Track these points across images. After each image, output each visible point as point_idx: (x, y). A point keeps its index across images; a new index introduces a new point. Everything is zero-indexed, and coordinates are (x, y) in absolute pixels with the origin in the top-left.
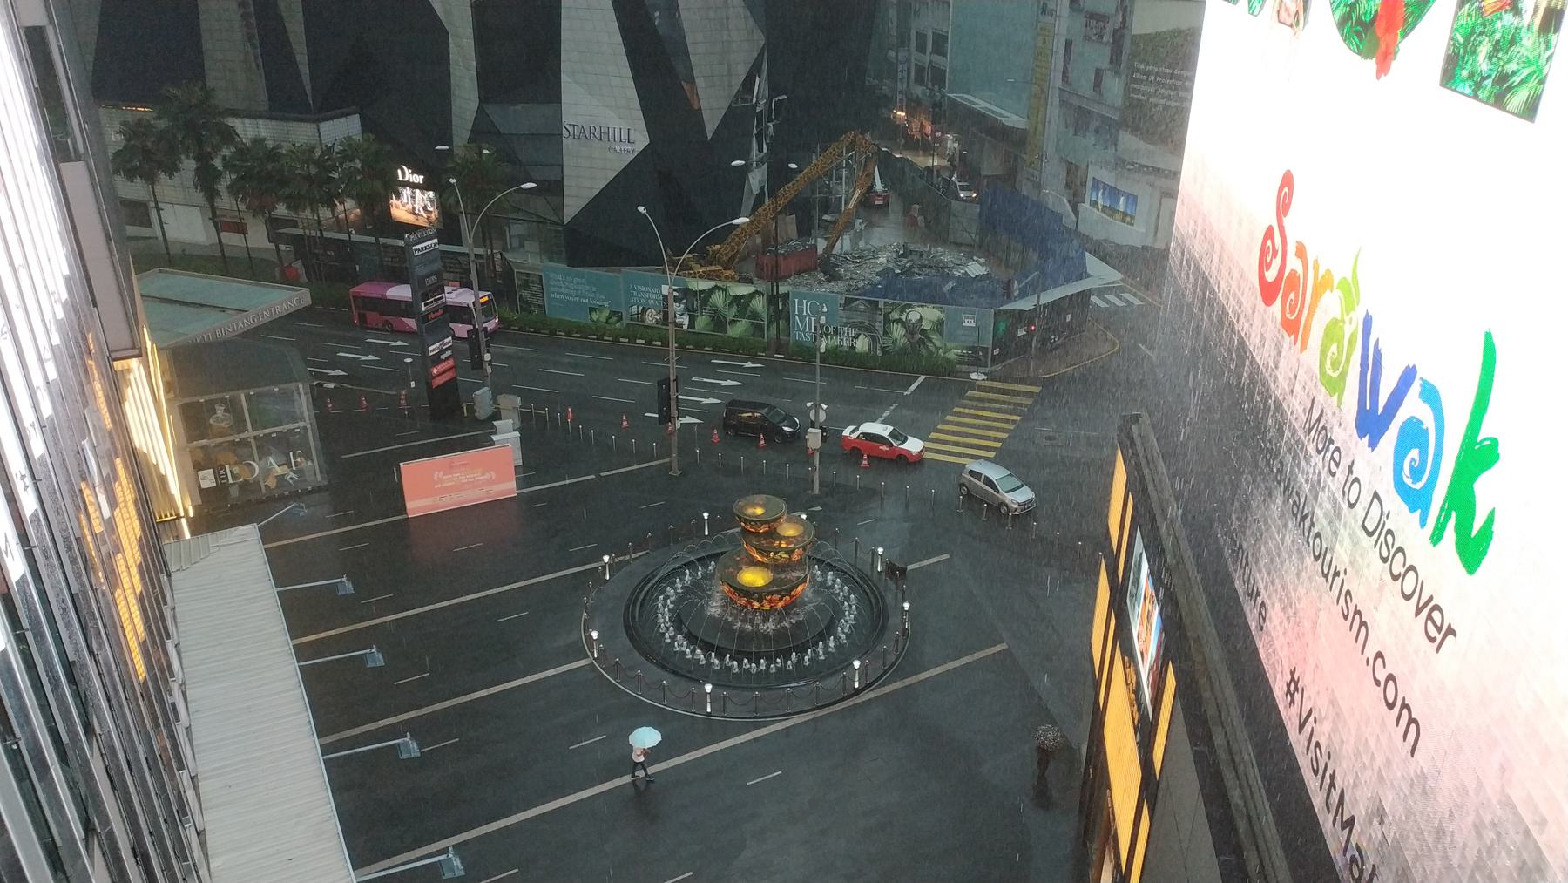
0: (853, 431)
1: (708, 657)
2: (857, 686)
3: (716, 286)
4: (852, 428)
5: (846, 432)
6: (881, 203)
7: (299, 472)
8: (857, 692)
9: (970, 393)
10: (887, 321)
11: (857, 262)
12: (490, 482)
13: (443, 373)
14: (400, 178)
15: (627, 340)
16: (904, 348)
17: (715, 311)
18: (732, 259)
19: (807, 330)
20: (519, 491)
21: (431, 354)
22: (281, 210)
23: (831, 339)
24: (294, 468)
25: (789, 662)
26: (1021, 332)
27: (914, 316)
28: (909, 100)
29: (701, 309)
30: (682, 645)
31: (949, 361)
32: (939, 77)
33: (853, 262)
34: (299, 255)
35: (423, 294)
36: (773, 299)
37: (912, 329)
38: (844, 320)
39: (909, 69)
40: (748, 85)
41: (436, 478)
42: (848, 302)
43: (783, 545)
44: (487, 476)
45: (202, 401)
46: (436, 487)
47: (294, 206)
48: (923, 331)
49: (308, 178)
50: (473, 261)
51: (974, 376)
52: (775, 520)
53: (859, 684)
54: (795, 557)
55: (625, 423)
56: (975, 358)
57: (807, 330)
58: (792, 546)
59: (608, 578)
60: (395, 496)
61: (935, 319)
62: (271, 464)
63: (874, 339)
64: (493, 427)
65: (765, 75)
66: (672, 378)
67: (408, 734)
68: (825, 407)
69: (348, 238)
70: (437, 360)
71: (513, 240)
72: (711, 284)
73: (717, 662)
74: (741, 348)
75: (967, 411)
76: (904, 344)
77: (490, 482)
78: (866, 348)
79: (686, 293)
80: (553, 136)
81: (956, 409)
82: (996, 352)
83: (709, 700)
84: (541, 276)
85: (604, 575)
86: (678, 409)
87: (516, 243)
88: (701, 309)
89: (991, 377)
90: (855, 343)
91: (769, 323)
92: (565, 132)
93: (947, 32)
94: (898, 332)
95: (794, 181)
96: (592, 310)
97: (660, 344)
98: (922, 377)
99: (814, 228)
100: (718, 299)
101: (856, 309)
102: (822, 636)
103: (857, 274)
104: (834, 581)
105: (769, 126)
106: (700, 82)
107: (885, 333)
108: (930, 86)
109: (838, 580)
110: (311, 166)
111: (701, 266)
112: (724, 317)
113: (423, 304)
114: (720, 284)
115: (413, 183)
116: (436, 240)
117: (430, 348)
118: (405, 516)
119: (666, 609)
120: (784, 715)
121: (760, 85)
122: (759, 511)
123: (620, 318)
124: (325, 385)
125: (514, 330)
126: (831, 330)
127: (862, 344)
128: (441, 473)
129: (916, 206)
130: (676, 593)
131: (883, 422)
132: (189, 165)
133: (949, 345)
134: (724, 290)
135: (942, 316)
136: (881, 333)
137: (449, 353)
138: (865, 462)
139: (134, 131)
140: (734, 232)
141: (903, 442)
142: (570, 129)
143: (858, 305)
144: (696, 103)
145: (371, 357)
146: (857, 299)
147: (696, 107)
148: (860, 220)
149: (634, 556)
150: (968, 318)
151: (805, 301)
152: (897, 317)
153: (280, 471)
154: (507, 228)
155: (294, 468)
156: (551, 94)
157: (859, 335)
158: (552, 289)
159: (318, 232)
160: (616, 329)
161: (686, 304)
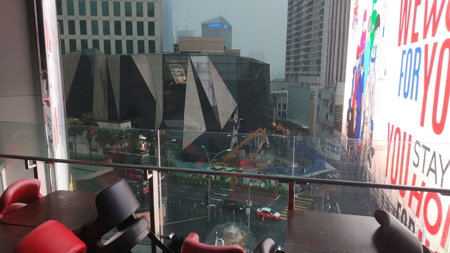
0: (260, 210)
5: (258, 210)
18: (227, 161)
21: (144, 185)
23: (254, 183)
32: (284, 114)
40: (233, 116)
55: (195, 206)
63: (266, 184)
65: (237, 114)
68: (251, 202)
78: (264, 186)
82: (301, 189)
84: (175, 164)
89: (300, 196)
90: (261, 185)
92: (184, 127)
98: (280, 195)
107: (269, 182)
108: (282, 117)
114: (223, 167)
117: (144, 183)
121: (236, 116)
131: (268, 208)
136: (268, 182)
138: (263, 219)
141: (274, 214)
146: (261, 173)
148: (263, 151)
156: (182, 118)
157: (262, 182)
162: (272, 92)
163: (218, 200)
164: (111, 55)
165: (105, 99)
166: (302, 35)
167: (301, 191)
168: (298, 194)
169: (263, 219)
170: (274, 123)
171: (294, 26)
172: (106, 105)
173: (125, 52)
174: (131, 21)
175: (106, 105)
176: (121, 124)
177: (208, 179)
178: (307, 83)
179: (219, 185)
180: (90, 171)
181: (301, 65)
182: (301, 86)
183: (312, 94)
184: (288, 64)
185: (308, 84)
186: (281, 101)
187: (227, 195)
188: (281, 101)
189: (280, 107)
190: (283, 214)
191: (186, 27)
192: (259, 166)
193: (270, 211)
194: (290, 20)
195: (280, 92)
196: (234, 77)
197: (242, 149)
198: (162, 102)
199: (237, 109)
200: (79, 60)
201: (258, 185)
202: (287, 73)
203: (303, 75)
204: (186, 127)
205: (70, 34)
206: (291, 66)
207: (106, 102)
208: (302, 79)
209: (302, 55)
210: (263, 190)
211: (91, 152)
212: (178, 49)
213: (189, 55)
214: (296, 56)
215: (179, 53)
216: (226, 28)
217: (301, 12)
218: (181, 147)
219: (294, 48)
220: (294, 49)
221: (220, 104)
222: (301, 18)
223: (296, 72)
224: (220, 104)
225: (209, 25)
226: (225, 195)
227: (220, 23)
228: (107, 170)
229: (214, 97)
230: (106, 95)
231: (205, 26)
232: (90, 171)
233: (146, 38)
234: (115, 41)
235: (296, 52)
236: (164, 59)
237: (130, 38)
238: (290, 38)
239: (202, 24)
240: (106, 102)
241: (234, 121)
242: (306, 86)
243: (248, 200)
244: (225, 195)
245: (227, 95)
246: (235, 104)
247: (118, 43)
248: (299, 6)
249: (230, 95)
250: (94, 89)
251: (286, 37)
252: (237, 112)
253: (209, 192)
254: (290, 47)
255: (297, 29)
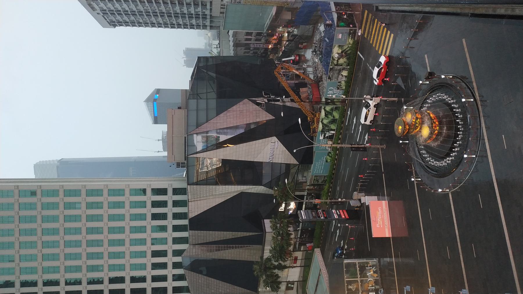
0: (376, 81)
1: (454, 152)
2: (472, 100)
3: (324, 109)
4: (374, 81)
5: (376, 83)
6: (298, 57)
7: (373, 266)
8: (475, 100)
9: (366, 36)
10: (337, 65)
11: (317, 70)
12: (382, 209)
13: (344, 213)
14: (283, 210)
15: (334, 171)
16: (348, 59)
17: (330, 122)
18: (313, 114)
19: (338, 92)
20: (386, 200)
21: (338, 217)
22: (291, 248)
23: (342, 84)
24: (371, 268)
25: (460, 123)
26: (345, 17)
27: (336, 56)
28: (266, 43)
29: (329, 127)
30: (449, 160)
31: (353, 43)
32: (259, 34)
33: (317, 71)
34: (305, 245)
35: (318, 218)
36: (327, 103)
37: (341, 56)
38: (336, 80)
39: (256, 44)
40: (258, 104)
41: (379, 227)
42: (329, 78)
43: (414, 120)
44: (380, 210)
45: (346, 284)
46: (382, 227)
47: (290, 245)
48: (342, 52)
49: (282, 239)
50: (309, 201)
51: (360, 34)
52: (404, 122)
53: (472, 99)
54: (419, 116)
55: (366, 159)
56: (353, 34)
57: (338, 92)
58: (415, 118)
59: (420, 179)
60: (384, 240)
61: (338, 48)
62: (369, 275)
63: (344, 69)
64: (364, 203)
65: (256, 99)
66: (351, 146)
67: (459, 292)
68: (365, 96)
69: (300, 231)
70: (340, 216)
71: (303, 179)
72: (320, 123)
73: (456, 149)
74: (343, 115)
75: (372, 39)
76: (346, 59)
77: (382, 209)
78: (347, 72)
79: (323, 131)
80: (273, 165)
81: (371, 42)
82: (351, 26)
83: (470, 156)
84: (315, 176)
85: (419, 181)
86: (362, 145)
87: (304, 179)
88: (329, 127)
89: (360, 28)
90: (344, 76)
91: (335, 104)
92: (271, 161)
93: (245, 32)
94: (341, 61)
95: (289, 92)
96: (327, 161)
97: (339, 141)
98: (358, 53)
99: (304, 82)
100: (325, 122)
101: (332, 76)
102: (452, 109)
103: (321, 70)
104: (431, 100)
105: (272, 97)
106: (258, 120)
107: (341, 65)
108: (262, 37)
109: (430, 98)
110: (278, 238)
111: (314, 124)
112: (332, 120)
113: (321, 218)
114: (320, 121)
115: (285, 207)
116: (302, 211)
117: (336, 217)
118: (391, 238)
119: (434, 162)
120: (480, 129)
121: (259, 100)
122: (400, 127)
123: (330, 153)
124: (346, 248)
125: (332, 186)
126: (339, 84)
127: (345, 73)
128: (377, 224)
129: (300, 46)
130: (429, 157)
131: (373, 70)
132: (276, 271)
133: (348, 43)
134: (323, 119)
135: (337, 46)
136: (341, 67)
137: (338, 211)
138: (387, 79)
139: (266, 285)
140: (304, 112)
141: (382, 64)
142: (270, 160)
143: (331, 75)
144: (264, 121)
145: (338, 231)
146: (329, 75)
147: (265, 122)
148: (303, 65)
149: (413, 168)
150: (338, 37)
151: (328, 93)
152: (336, 61)
153: (372, 272)
154: (300, 181)
155: (371, 268)
156: (261, 163)
157: (341, 75)
158: (319, 173)
159: (298, 239)
160: (333, 154)
161: (327, 132)
162: (232, 53)
163: (360, 130)
164: (189, 237)
165: (238, 247)
166: (164, 11)
167: (355, 26)
168: (357, 29)
169: (387, 79)
170: (269, 46)
171: (153, 19)
172: (245, 247)
173: (185, 222)
174: (151, 264)
175: (245, 246)
176: (267, 231)
177: (329, 202)
178: (221, 8)
179: (342, 126)
180: (320, 275)
181: (199, 12)
182: (224, 14)
183: (234, 3)
184: (198, 27)
185: (222, 7)
186: (242, 38)
187: (355, 118)
188: (242, 38)
189: (250, 40)
190: (382, 52)
191: (159, 140)
192: (320, 73)
193: (378, 68)
194: (146, 25)
195: (231, 39)
196: (213, 103)
197: (300, 91)
198: (242, 186)
199: (250, 99)
200: (195, 273)
201: (344, 79)
202: (208, 28)
203: (211, 9)
204: (272, 159)
205: (166, 281)
206: (200, 23)
207: (241, 247)
208: (216, 11)
209: (187, 10)
210: (351, 73)
211: (297, 282)
212: (182, 163)
213: (187, 156)
214: (189, 17)
215: (186, 162)
216: (158, 95)
217: (136, 11)
218: (295, 165)
219: (179, 19)
220: (180, 19)
221: (245, 119)
222: (144, 11)
223: (208, 17)
224: (245, 119)
225: (155, 116)
226: (355, 121)
227: (153, 104)
228: (319, 256)
229: (237, 127)
230: (234, 247)
231: (156, 121)
232: (320, 275)
233: (170, 198)
234: (173, 270)
235: (183, 17)
236: (193, 184)
237: (170, 216)
238: (168, 24)
239: (155, 124)
240: (242, 246)
241: (265, 102)
242: (225, 6)
243: (362, 100)
244: (355, 121)
245: (234, 111)
246: (245, 102)
247: (176, 228)
248: (130, 13)
249: (234, 107)
250: (227, 258)
251: (167, 29)
252: (254, 99)
253: (350, 146)
254: (178, 25)
255: (157, 16)
